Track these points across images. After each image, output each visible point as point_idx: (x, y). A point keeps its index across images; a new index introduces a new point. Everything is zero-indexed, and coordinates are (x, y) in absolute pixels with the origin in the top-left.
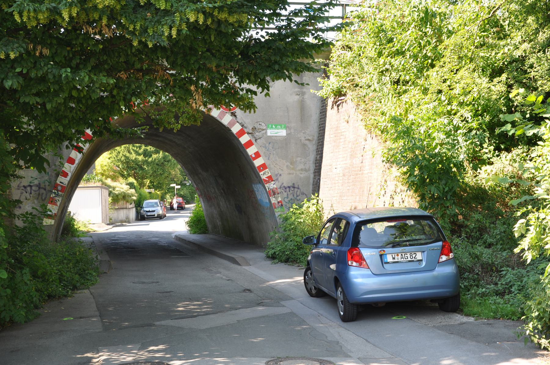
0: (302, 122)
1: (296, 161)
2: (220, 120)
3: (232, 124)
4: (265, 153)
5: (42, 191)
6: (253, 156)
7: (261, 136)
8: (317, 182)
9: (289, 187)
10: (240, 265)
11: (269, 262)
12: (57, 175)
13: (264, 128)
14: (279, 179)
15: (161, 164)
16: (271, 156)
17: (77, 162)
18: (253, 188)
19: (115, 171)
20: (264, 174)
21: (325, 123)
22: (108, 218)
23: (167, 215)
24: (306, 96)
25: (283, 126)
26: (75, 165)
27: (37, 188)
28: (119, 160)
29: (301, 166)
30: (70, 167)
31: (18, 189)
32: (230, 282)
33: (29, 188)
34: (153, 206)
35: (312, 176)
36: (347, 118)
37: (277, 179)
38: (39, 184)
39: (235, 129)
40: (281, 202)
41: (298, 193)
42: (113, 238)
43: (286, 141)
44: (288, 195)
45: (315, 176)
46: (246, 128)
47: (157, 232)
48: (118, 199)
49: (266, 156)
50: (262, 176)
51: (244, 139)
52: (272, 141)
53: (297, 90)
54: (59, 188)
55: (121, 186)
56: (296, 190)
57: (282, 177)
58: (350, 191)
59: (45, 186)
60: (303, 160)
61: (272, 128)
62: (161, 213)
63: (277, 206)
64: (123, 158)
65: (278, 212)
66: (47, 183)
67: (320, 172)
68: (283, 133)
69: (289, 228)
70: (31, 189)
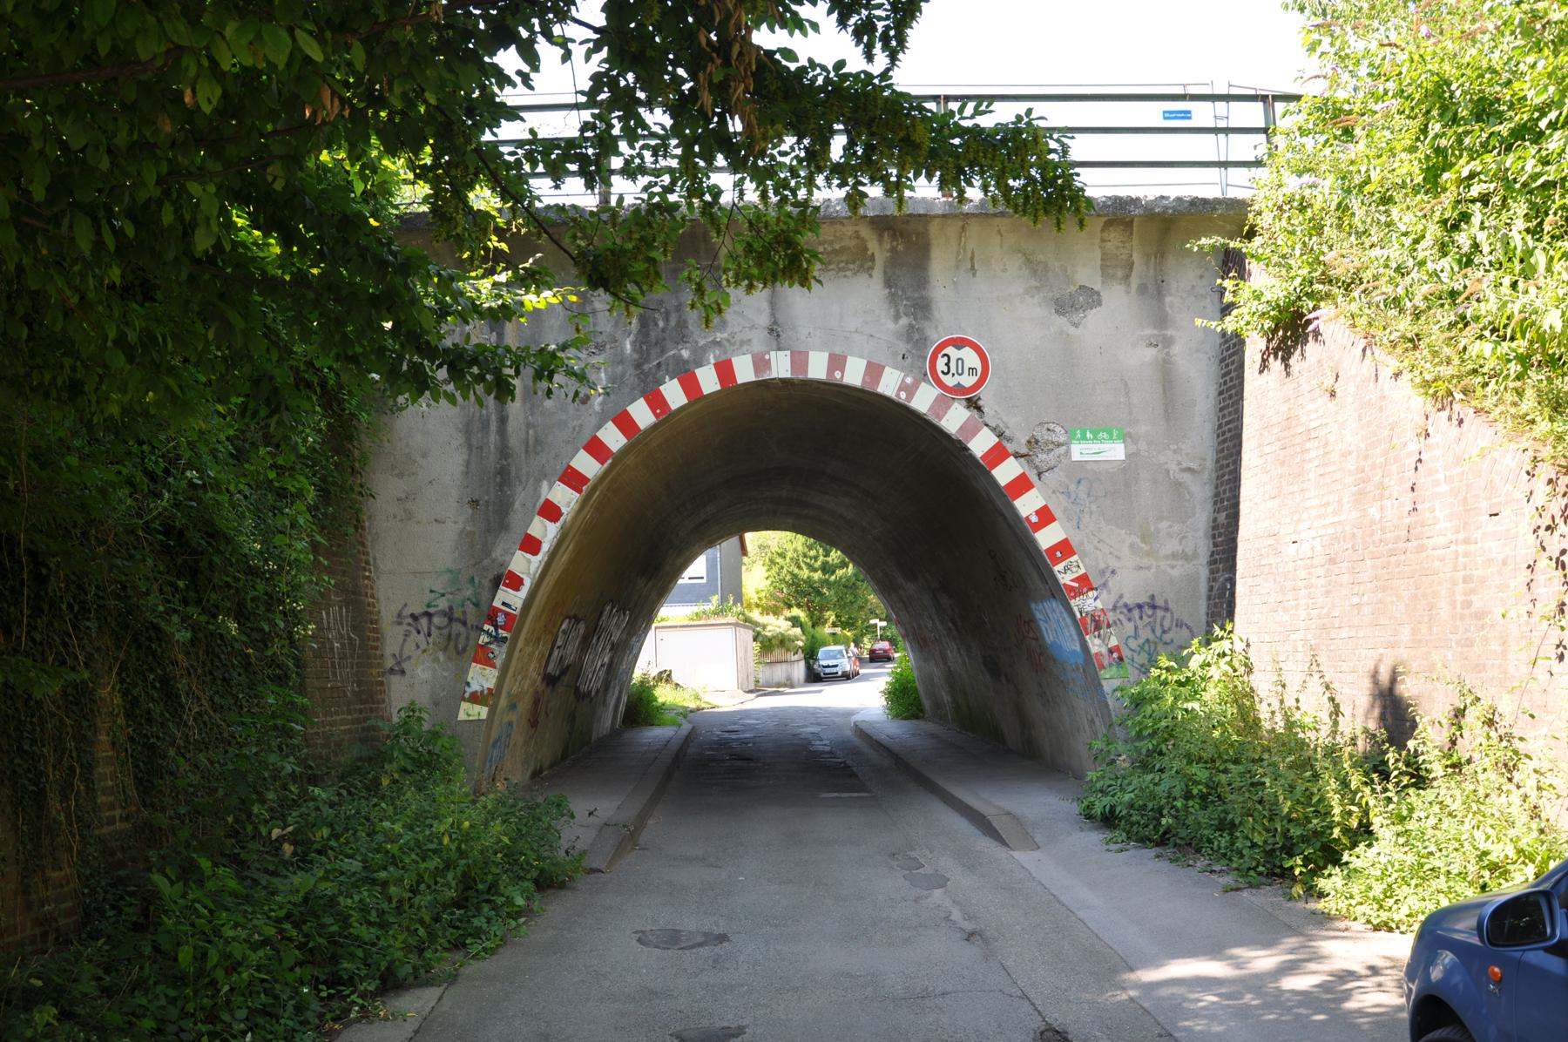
1: (1158, 531)
2: (935, 421)
3: (971, 429)
4: (1066, 510)
5: (457, 628)
6: (1034, 519)
7: (1053, 463)
8: (1223, 588)
9: (1140, 607)
10: (1004, 843)
12: (496, 583)
13: (1062, 439)
15: (849, 586)
16: (1086, 518)
17: (545, 547)
18: (1033, 615)
19: (777, 599)
20: (1066, 569)
21: (1240, 419)
22: (752, 679)
24: (1176, 349)
25: (1115, 433)
27: (446, 620)
29: (1172, 546)
30: (529, 561)
31: (400, 623)
32: (971, 952)
33: (424, 621)
34: (835, 658)
35: (1204, 573)
36: (1329, 382)
37: (1105, 585)
38: (451, 608)
39: (980, 445)
40: (1117, 649)
41: (1167, 624)
42: (735, 727)
43: (1126, 472)
44: (1136, 628)
45: (1212, 572)
46: (1009, 440)
47: (826, 710)
48: (769, 646)
49: (1069, 519)
50: (1059, 576)
51: (1005, 473)
52: (1084, 474)
53: (1148, 331)
54: (501, 619)
55: (777, 625)
56: (1160, 613)
57: (1118, 578)
58: (1366, 609)
59: (464, 613)
60: (1176, 528)
61: (1084, 438)
63: (1106, 662)
64: (788, 578)
65: (1110, 680)
66: (470, 607)
67: (1234, 558)
68: (1115, 451)
69: (1158, 740)
70: (430, 622)
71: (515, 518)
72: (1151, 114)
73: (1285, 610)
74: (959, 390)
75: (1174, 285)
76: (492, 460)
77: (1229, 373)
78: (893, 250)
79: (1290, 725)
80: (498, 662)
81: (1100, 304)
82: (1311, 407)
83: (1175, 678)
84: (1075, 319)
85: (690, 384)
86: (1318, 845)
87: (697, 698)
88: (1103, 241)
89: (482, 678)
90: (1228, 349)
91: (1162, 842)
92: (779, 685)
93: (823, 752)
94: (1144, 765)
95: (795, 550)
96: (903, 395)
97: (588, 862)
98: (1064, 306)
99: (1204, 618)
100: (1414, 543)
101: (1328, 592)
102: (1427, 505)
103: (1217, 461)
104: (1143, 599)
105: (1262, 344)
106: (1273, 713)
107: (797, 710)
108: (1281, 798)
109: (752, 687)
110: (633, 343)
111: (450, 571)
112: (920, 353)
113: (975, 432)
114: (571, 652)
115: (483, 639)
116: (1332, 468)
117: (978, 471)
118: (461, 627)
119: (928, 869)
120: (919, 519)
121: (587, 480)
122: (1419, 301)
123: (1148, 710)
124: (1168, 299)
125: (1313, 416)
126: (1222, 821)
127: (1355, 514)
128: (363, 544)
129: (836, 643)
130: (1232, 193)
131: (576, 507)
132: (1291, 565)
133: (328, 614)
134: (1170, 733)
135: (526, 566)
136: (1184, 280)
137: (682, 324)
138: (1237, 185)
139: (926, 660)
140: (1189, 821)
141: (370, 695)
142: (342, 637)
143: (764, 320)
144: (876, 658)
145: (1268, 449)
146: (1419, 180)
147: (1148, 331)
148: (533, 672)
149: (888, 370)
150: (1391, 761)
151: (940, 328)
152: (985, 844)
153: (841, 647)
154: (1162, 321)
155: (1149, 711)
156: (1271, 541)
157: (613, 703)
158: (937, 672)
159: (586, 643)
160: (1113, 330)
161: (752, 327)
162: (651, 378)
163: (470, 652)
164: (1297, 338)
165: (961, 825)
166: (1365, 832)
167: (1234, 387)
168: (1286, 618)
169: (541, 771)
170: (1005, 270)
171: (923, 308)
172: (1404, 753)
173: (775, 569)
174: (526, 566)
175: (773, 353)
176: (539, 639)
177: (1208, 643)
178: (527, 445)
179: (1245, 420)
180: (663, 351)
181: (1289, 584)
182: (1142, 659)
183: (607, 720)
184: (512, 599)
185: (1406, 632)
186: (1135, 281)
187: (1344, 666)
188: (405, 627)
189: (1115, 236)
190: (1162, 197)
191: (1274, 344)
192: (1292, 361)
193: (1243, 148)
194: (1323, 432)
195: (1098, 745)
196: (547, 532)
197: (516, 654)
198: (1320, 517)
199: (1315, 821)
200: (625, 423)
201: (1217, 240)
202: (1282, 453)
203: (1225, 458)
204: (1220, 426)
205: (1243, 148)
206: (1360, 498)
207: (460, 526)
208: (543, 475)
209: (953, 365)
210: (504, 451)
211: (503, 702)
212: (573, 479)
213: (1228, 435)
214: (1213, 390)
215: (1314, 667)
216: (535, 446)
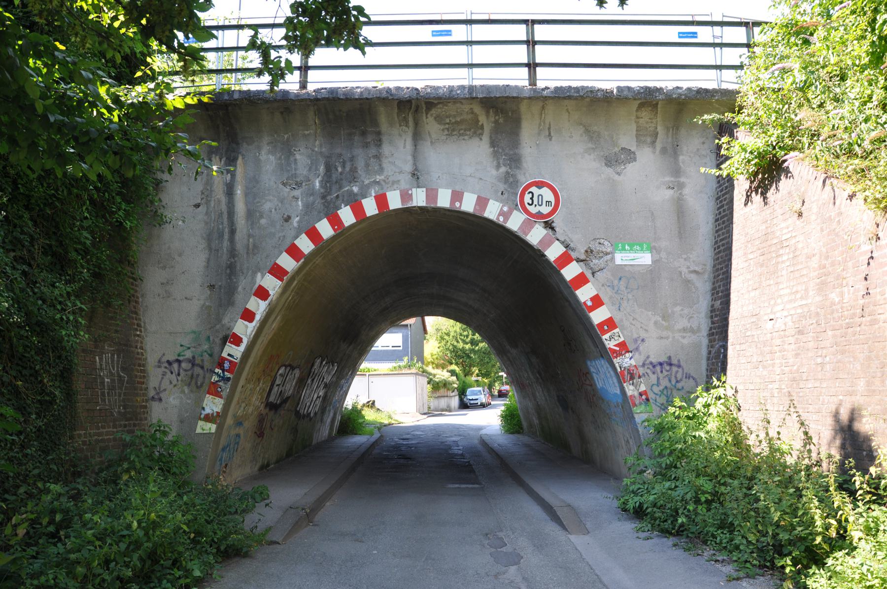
0: (681, 238)
1: (673, 313)
4: (611, 297)
5: (197, 370)
6: (589, 303)
8: (719, 352)
9: (661, 364)
11: (628, 526)
13: (609, 250)
14: (641, 348)
17: (258, 317)
20: (611, 338)
22: (426, 407)
23: (492, 403)
24: (686, 191)
26: (254, 323)
27: (190, 365)
28: (448, 349)
29: (683, 323)
30: (247, 327)
31: (159, 367)
33: (176, 366)
35: (705, 342)
36: (798, 206)
37: (637, 349)
38: (194, 357)
39: (553, 253)
40: (645, 393)
41: (679, 376)
42: (408, 436)
43: (651, 275)
44: (658, 379)
45: (710, 341)
48: (437, 387)
49: (613, 304)
50: (606, 343)
51: (570, 272)
52: (624, 274)
53: (668, 179)
54: (227, 365)
55: (442, 375)
56: (674, 369)
57: (646, 344)
59: (203, 361)
60: (686, 311)
61: (624, 249)
62: (484, 401)
63: (637, 402)
65: (640, 414)
66: (206, 357)
68: (645, 259)
69: (674, 457)
70: (180, 366)
71: (239, 297)
72: (671, 34)
73: (764, 367)
74: (539, 215)
75: (685, 148)
76: (224, 258)
77: (722, 206)
78: (496, 122)
79: (773, 450)
80: (224, 394)
81: (635, 160)
82: (783, 225)
83: (686, 414)
84: (619, 169)
85: (358, 210)
86: (803, 548)
87: (390, 417)
88: (638, 117)
89: (213, 405)
90: (722, 191)
91: (680, 532)
92: (443, 410)
93: (457, 455)
94: (663, 474)
95: (455, 332)
96: (501, 219)
97: (270, 537)
98: (611, 161)
99: (704, 373)
100: (868, 319)
101: (797, 355)
102: (878, 290)
103: (714, 266)
104: (663, 359)
105: (747, 185)
106: (760, 442)
107: (440, 426)
108: (773, 509)
109: (426, 411)
110: (321, 182)
111: (194, 332)
112: (513, 190)
113: (549, 244)
114: (289, 388)
115: (215, 378)
116: (800, 267)
117: (551, 271)
118: (202, 369)
119: (508, 549)
120: (522, 307)
121: (287, 273)
122: (867, 145)
123: (667, 436)
124: (681, 158)
125: (785, 231)
126: (722, 521)
127: (818, 299)
128: (136, 313)
129: (478, 386)
130: (724, 86)
131: (280, 291)
132: (769, 335)
133: (101, 359)
134: (682, 454)
135: (245, 330)
136: (693, 146)
137: (354, 170)
138: (728, 80)
139: (524, 397)
140: (698, 519)
141: (134, 414)
142: (112, 374)
143: (408, 167)
144: (502, 395)
145: (751, 256)
146: (866, 60)
147: (668, 179)
148: (256, 402)
149: (491, 202)
150: (858, 484)
151: (527, 175)
152: (552, 528)
153: (480, 389)
154: (677, 172)
155: (667, 437)
156: (754, 319)
157: (329, 420)
158: (530, 405)
159: (301, 383)
160: (644, 176)
161: (400, 172)
162: (332, 205)
163: (206, 387)
164: (773, 178)
165: (536, 511)
166: (841, 541)
167: (726, 215)
168: (765, 373)
169: (268, 465)
170: (571, 137)
171: (515, 161)
172: (867, 477)
173: (443, 343)
174: (245, 330)
175: (414, 190)
176: (259, 380)
177: (707, 390)
178: (248, 249)
179: (734, 237)
180: (341, 188)
181: (767, 349)
182: (663, 400)
183: (324, 432)
184: (236, 352)
185: (861, 385)
186: (659, 145)
187: (811, 408)
188: (163, 369)
189: (645, 114)
190: (678, 88)
191: (755, 184)
192: (768, 195)
193: (732, 56)
194: (793, 241)
195: (631, 460)
196: (260, 307)
197: (239, 389)
198: (791, 301)
199: (800, 529)
200: (313, 235)
201: (716, 116)
202: (762, 258)
203: (720, 264)
204: (716, 242)
205: (732, 56)
206: (822, 287)
207: (202, 302)
208: (258, 269)
209: (535, 199)
210: (233, 253)
211: (229, 421)
212: (278, 272)
213: (722, 248)
214: (711, 219)
215: (792, 409)
216: (254, 249)
